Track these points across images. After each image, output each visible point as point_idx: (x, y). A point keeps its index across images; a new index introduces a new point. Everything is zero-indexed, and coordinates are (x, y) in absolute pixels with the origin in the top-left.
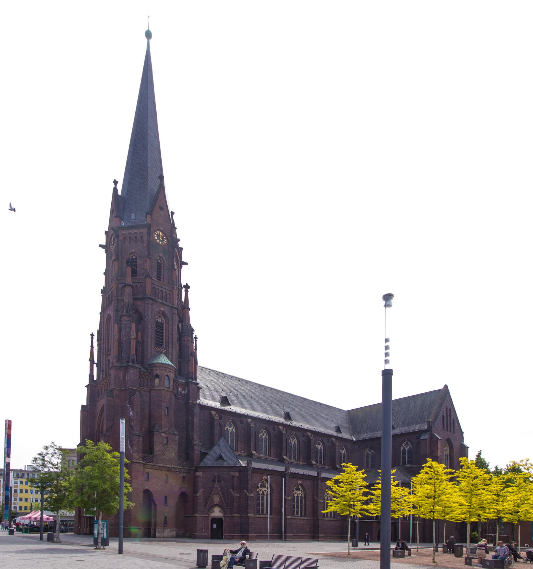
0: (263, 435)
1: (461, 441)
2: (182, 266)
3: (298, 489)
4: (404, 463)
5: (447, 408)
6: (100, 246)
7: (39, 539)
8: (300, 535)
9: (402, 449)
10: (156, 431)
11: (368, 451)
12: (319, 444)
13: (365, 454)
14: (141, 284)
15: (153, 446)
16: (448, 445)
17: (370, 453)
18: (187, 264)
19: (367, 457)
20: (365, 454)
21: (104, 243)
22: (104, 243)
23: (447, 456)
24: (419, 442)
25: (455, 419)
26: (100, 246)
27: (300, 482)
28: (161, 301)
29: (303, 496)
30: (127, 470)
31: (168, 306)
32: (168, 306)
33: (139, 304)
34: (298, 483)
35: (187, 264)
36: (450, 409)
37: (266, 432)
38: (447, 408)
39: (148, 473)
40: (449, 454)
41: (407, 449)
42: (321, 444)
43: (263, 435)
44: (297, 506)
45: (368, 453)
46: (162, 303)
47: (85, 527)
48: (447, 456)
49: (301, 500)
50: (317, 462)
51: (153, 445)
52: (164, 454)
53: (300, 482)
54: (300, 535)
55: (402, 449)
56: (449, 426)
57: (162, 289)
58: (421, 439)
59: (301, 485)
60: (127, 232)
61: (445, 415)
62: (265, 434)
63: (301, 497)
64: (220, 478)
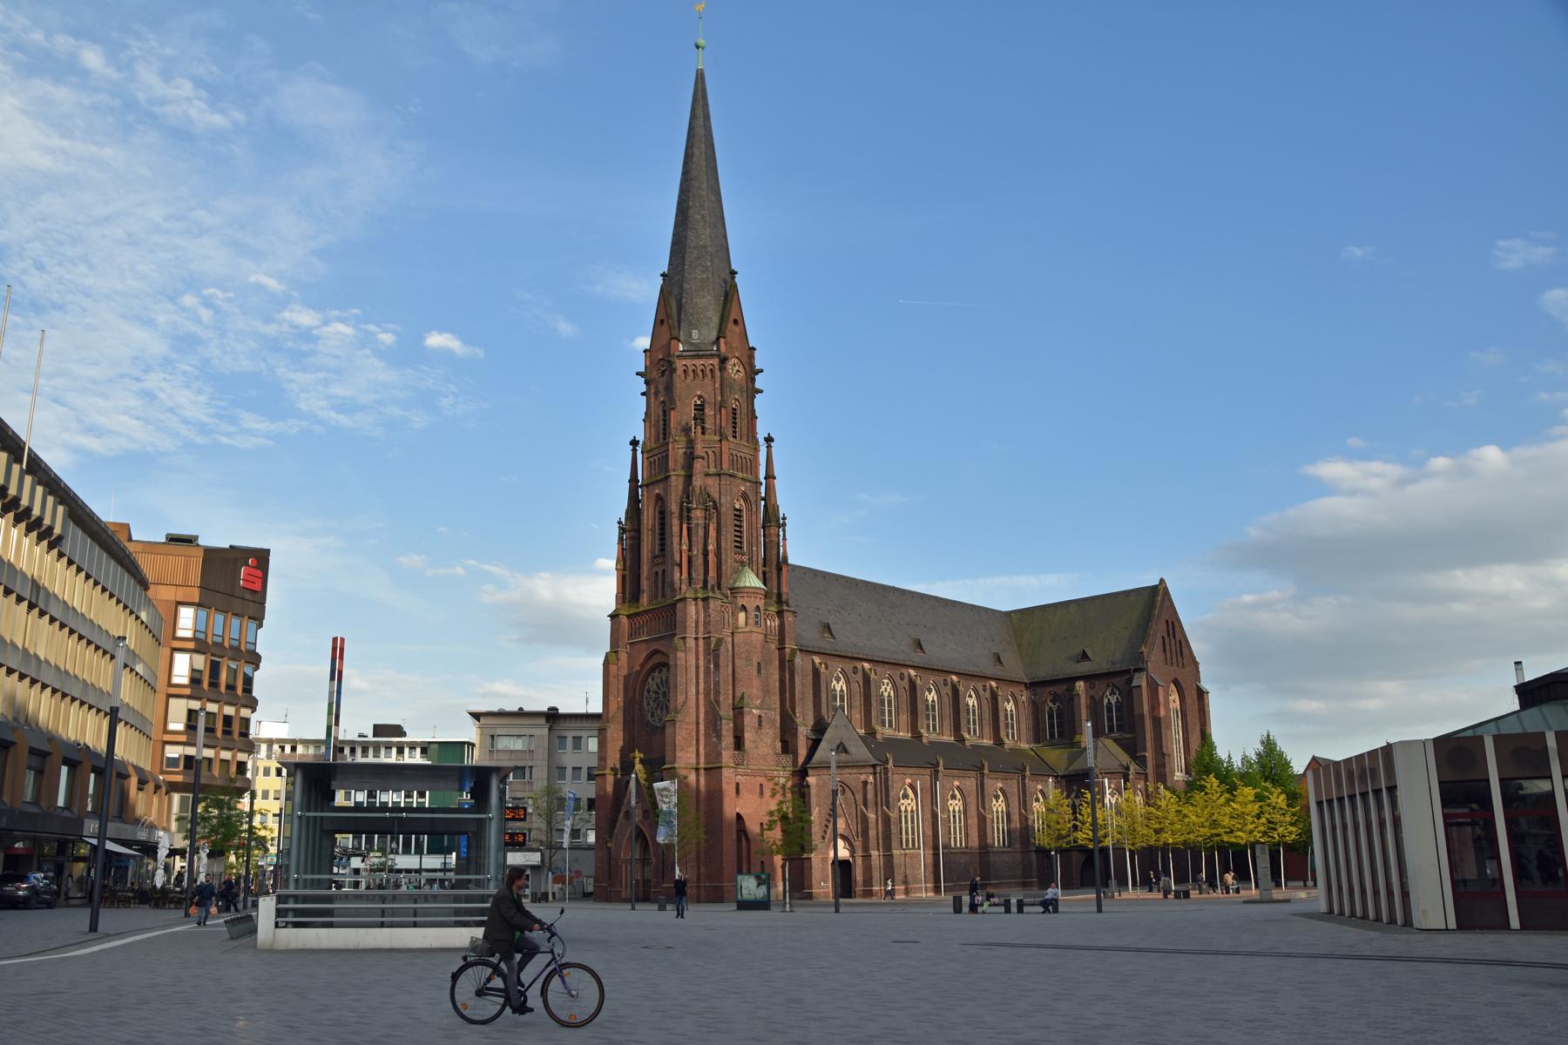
0: (886, 690)
1: (1196, 680)
2: (755, 397)
3: (954, 797)
4: (1111, 730)
5: (1167, 622)
6: (637, 374)
7: (952, 910)
8: (963, 883)
9: (1106, 701)
10: (1387, 1037)
11: (1051, 705)
12: (970, 696)
13: (1047, 709)
14: (714, 449)
15: (743, 735)
16: (1176, 691)
17: (1055, 708)
18: (761, 391)
19: (1051, 717)
20: (1047, 709)
21: (642, 370)
22: (642, 370)
23: (1177, 712)
24: (1131, 690)
25: (1183, 641)
26: (637, 374)
27: (957, 783)
28: (740, 475)
29: (962, 808)
30: (642, 755)
31: (750, 481)
32: (750, 481)
33: (711, 483)
34: (953, 785)
35: (761, 391)
36: (1172, 623)
37: (890, 684)
38: (1167, 622)
39: (738, 784)
40: (1179, 708)
41: (1113, 702)
42: (974, 696)
43: (886, 690)
44: (955, 828)
45: (1050, 708)
46: (743, 479)
47: (624, 886)
48: (1177, 712)
49: (960, 816)
50: (969, 733)
51: (743, 731)
52: (757, 747)
53: (957, 783)
54: (963, 883)
55: (1106, 701)
56: (1174, 656)
57: (742, 454)
58: (1133, 685)
59: (959, 788)
60: (689, 362)
61: (1166, 635)
62: (888, 688)
63: (959, 811)
64: (844, 786)
